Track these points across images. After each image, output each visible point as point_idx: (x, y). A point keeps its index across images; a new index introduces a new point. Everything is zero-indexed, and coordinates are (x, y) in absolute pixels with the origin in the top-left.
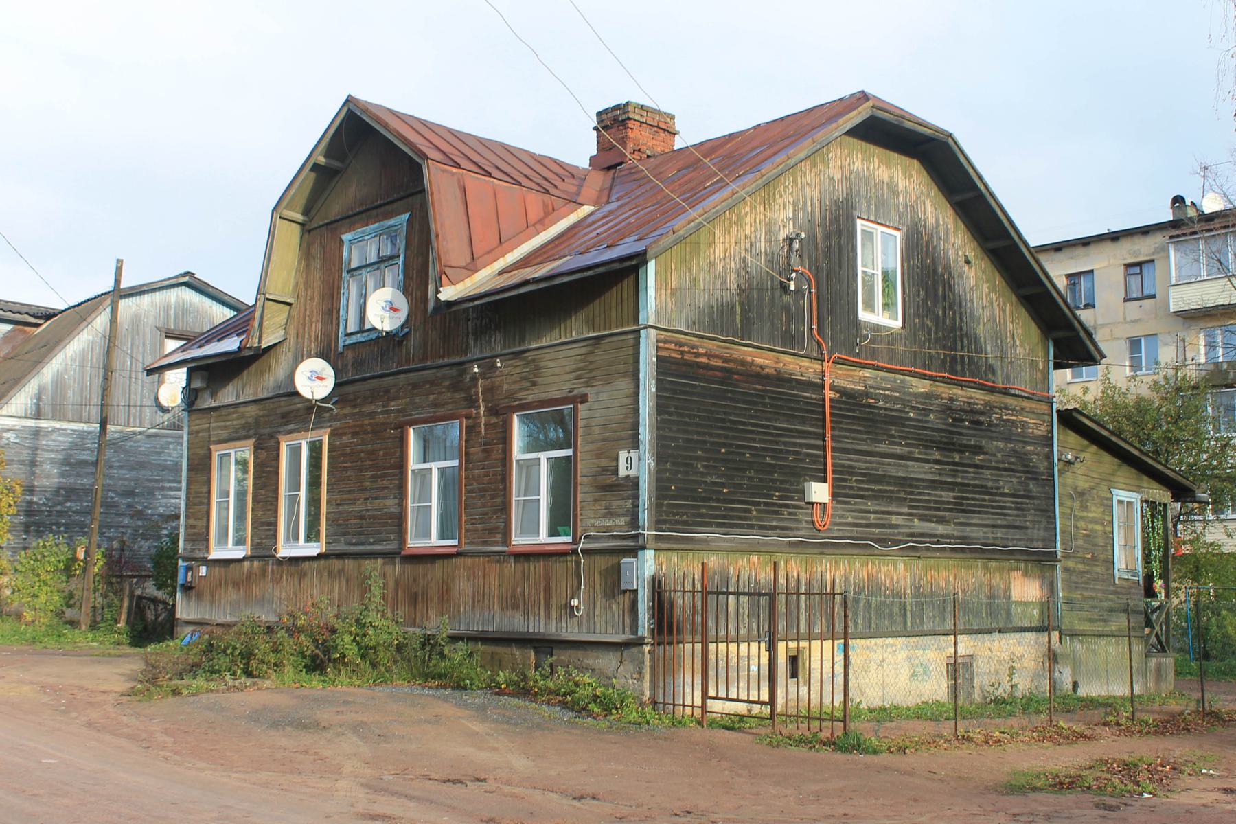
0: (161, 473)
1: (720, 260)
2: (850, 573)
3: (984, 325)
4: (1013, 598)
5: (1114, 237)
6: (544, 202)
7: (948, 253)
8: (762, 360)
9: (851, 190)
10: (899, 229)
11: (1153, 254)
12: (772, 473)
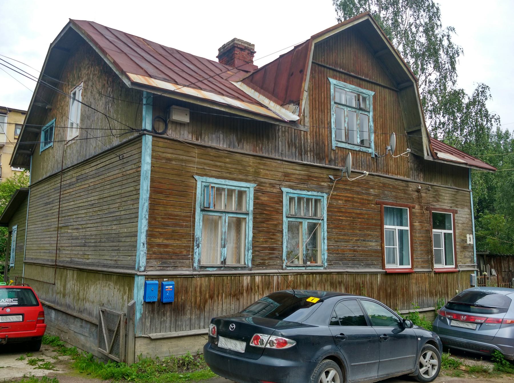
6: (250, 72)
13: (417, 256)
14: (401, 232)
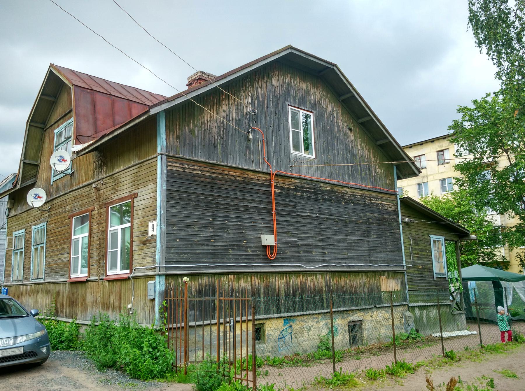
0: (420, 253)
1: (208, 122)
2: (290, 281)
3: (359, 158)
4: (382, 290)
5: (432, 141)
7: (339, 124)
8: (235, 173)
9: (285, 91)
10: (312, 112)
11: (448, 146)
12: (355, 241)
13: (93, 262)
14: (123, 230)
